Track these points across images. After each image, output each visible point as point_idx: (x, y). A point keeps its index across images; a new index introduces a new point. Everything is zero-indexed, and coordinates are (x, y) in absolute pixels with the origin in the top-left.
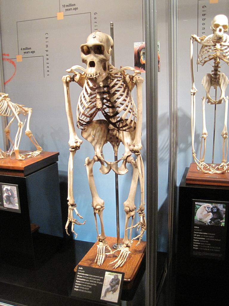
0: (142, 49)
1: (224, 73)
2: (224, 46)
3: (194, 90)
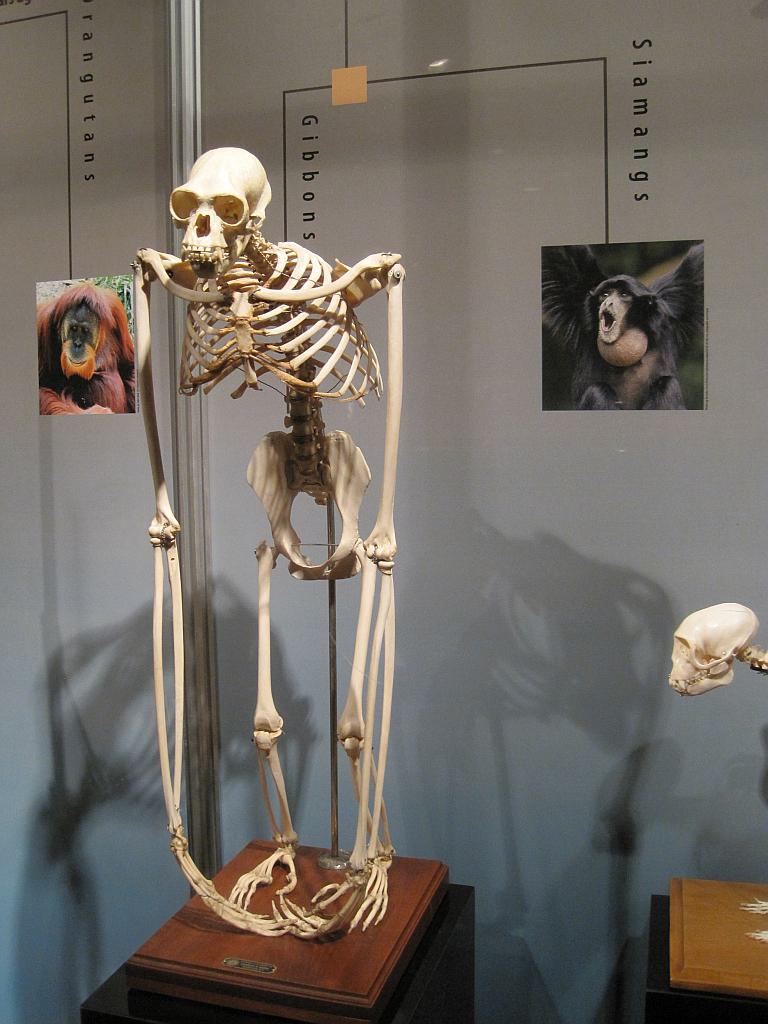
0: (68, 309)
1: (346, 431)
2: (274, 304)
3: (164, 521)
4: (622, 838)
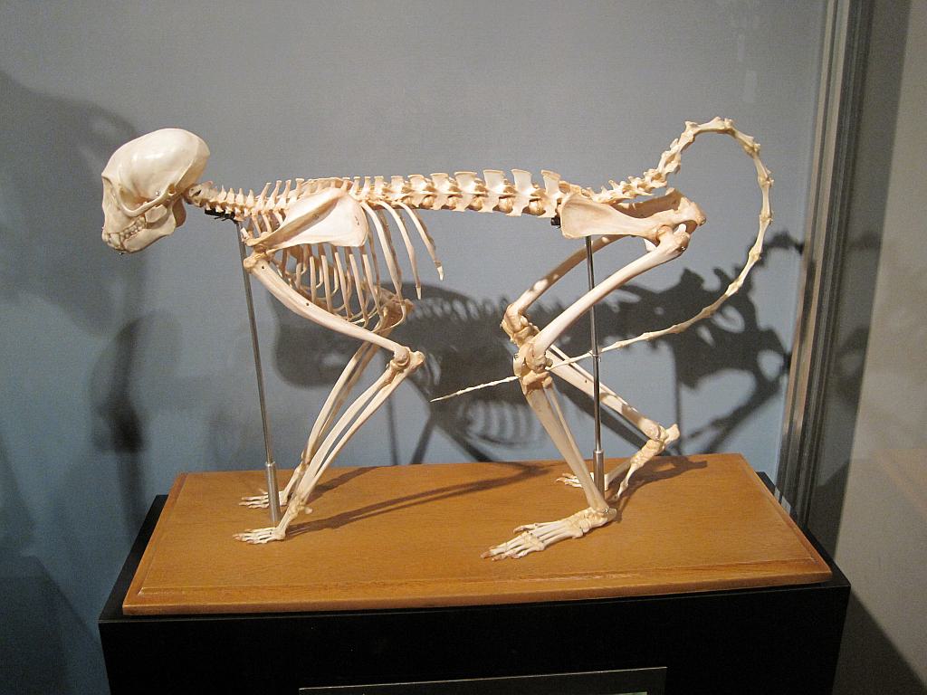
4: (125, 433)
